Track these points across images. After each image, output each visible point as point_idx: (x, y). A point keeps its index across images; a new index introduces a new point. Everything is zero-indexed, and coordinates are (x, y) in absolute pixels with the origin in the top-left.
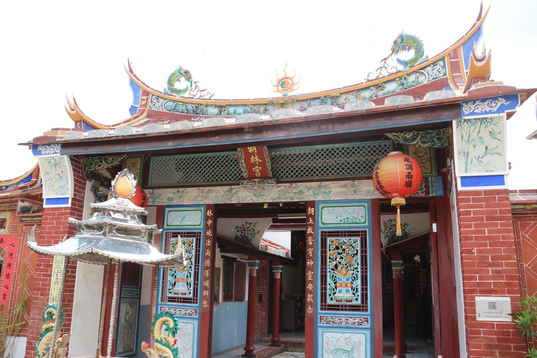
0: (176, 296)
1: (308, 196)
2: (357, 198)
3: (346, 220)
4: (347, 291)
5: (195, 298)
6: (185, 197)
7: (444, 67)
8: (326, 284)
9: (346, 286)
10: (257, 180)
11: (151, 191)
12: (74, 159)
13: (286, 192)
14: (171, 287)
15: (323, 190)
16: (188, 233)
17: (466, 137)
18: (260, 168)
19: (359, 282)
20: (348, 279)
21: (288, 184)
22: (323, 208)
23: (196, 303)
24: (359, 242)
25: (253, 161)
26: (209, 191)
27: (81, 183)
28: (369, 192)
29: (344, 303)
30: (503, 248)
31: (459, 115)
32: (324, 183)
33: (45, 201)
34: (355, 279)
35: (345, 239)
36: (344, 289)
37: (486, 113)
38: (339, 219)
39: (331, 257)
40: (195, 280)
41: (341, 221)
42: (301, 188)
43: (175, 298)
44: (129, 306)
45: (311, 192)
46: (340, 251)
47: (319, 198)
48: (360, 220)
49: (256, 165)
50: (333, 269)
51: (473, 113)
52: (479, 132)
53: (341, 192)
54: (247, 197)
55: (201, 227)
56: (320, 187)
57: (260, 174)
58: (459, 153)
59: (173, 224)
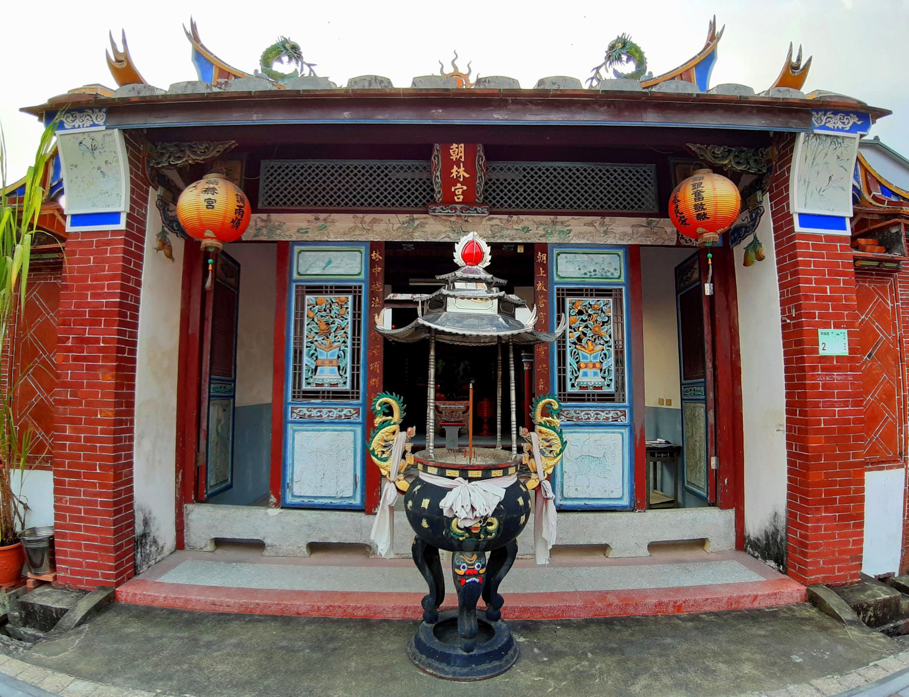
0: (319, 388)
1: (535, 236)
2: (609, 242)
3: (593, 274)
4: (595, 374)
5: (355, 390)
6: (330, 228)
8: (564, 365)
9: (594, 366)
10: (458, 207)
12: (132, 138)
13: (503, 229)
14: (310, 374)
15: (559, 227)
16: (337, 287)
18: (465, 188)
19: (611, 361)
20: (595, 358)
21: (506, 217)
22: (558, 254)
23: (358, 398)
25: (454, 175)
26: (374, 221)
27: (141, 188)
28: (625, 234)
29: (590, 390)
30: (846, 313)
31: (808, 126)
32: (560, 218)
33: (69, 219)
35: (592, 301)
36: (590, 372)
37: (838, 130)
38: (583, 271)
39: (573, 326)
40: (353, 362)
41: (585, 274)
42: (526, 223)
43: (318, 392)
44: (221, 409)
46: (585, 317)
47: (553, 239)
48: (612, 274)
49: (459, 182)
50: (574, 343)
51: (824, 127)
52: (826, 155)
53: (586, 233)
54: (439, 233)
55: (362, 277)
56: (554, 223)
57: (462, 197)
58: (799, 181)
59: (308, 273)
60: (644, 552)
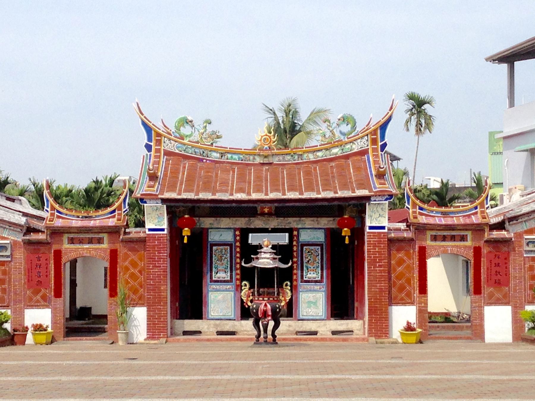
1: (294, 225)
7: (367, 140)
11: (197, 218)
17: (371, 210)
24: (320, 249)
26: (236, 220)
28: (325, 224)
32: (302, 219)
34: (318, 267)
36: (312, 273)
45: (295, 223)
47: (300, 226)
51: (375, 201)
60: (330, 336)
